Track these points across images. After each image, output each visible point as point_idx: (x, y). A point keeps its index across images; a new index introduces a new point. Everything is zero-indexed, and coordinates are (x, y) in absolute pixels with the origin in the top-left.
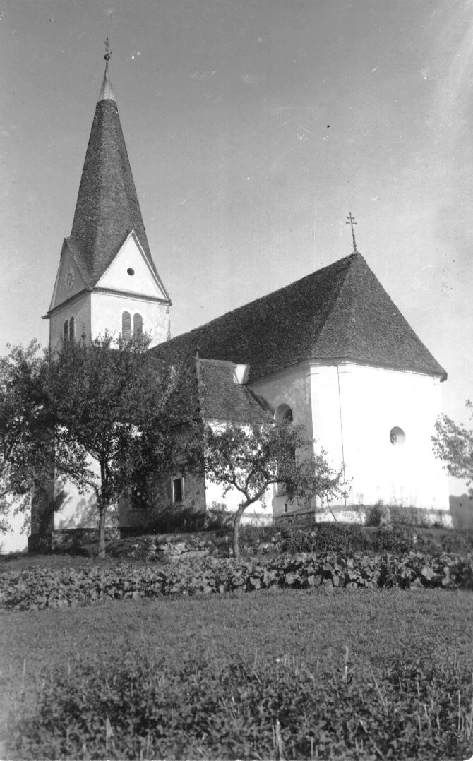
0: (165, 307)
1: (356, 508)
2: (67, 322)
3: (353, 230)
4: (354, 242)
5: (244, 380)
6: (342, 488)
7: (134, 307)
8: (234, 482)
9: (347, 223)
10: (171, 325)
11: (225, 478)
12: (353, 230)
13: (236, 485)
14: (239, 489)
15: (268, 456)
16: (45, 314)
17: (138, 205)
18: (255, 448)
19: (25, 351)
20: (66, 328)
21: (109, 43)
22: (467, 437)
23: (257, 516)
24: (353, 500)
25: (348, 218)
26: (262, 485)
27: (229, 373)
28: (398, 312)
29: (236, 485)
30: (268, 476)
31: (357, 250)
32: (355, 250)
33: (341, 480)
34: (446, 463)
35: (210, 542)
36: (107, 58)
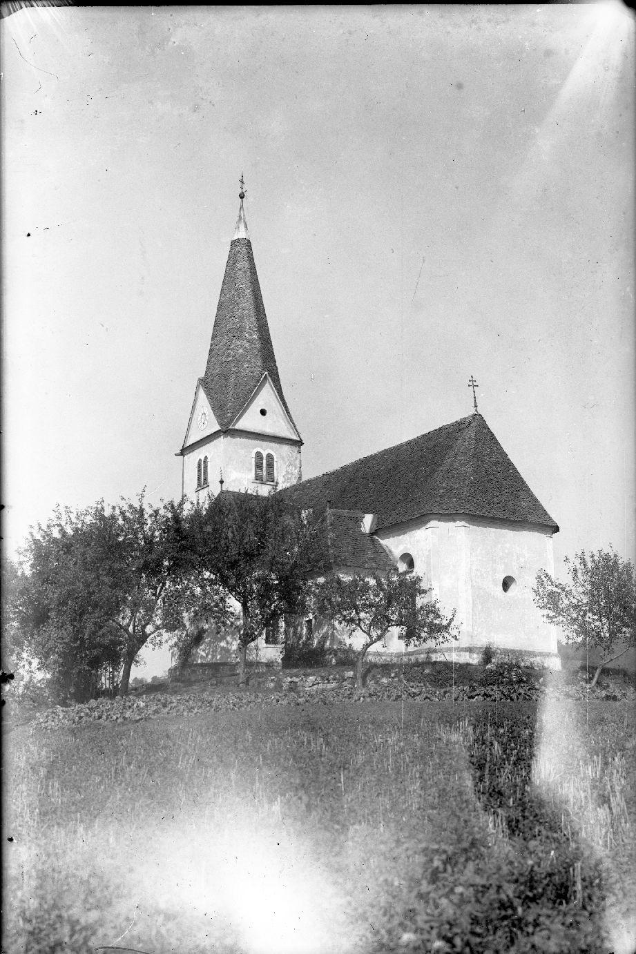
0: (296, 449)
1: (470, 650)
2: (200, 460)
3: (474, 392)
4: (475, 403)
5: (371, 529)
6: (454, 632)
7: (266, 449)
8: (359, 625)
9: (469, 386)
10: (302, 463)
11: (352, 621)
12: (474, 392)
13: (361, 627)
14: (363, 631)
15: (389, 604)
16: (179, 452)
17: (272, 345)
18: (377, 596)
19: (176, 504)
20: (199, 465)
21: (244, 181)
22: (563, 589)
23: (379, 654)
24: (464, 642)
25: (470, 381)
26: (384, 627)
27: (358, 521)
28: (514, 469)
29: (361, 627)
30: (389, 621)
31: (478, 410)
32: (476, 411)
33: (452, 626)
34: (545, 612)
35: (337, 676)
36: (242, 196)
